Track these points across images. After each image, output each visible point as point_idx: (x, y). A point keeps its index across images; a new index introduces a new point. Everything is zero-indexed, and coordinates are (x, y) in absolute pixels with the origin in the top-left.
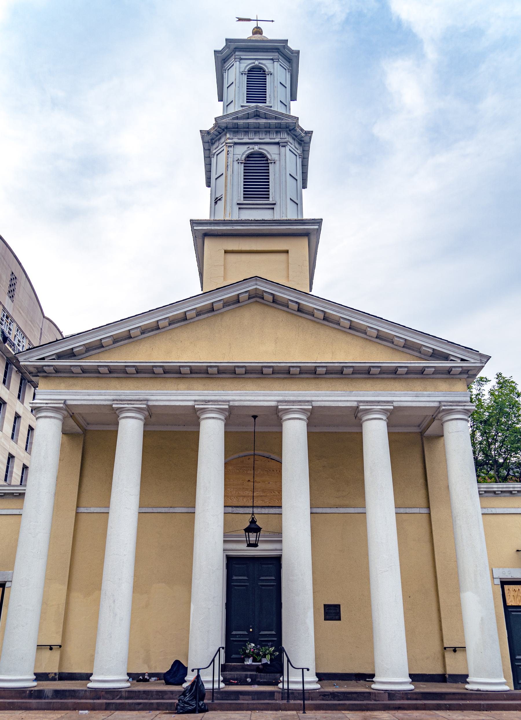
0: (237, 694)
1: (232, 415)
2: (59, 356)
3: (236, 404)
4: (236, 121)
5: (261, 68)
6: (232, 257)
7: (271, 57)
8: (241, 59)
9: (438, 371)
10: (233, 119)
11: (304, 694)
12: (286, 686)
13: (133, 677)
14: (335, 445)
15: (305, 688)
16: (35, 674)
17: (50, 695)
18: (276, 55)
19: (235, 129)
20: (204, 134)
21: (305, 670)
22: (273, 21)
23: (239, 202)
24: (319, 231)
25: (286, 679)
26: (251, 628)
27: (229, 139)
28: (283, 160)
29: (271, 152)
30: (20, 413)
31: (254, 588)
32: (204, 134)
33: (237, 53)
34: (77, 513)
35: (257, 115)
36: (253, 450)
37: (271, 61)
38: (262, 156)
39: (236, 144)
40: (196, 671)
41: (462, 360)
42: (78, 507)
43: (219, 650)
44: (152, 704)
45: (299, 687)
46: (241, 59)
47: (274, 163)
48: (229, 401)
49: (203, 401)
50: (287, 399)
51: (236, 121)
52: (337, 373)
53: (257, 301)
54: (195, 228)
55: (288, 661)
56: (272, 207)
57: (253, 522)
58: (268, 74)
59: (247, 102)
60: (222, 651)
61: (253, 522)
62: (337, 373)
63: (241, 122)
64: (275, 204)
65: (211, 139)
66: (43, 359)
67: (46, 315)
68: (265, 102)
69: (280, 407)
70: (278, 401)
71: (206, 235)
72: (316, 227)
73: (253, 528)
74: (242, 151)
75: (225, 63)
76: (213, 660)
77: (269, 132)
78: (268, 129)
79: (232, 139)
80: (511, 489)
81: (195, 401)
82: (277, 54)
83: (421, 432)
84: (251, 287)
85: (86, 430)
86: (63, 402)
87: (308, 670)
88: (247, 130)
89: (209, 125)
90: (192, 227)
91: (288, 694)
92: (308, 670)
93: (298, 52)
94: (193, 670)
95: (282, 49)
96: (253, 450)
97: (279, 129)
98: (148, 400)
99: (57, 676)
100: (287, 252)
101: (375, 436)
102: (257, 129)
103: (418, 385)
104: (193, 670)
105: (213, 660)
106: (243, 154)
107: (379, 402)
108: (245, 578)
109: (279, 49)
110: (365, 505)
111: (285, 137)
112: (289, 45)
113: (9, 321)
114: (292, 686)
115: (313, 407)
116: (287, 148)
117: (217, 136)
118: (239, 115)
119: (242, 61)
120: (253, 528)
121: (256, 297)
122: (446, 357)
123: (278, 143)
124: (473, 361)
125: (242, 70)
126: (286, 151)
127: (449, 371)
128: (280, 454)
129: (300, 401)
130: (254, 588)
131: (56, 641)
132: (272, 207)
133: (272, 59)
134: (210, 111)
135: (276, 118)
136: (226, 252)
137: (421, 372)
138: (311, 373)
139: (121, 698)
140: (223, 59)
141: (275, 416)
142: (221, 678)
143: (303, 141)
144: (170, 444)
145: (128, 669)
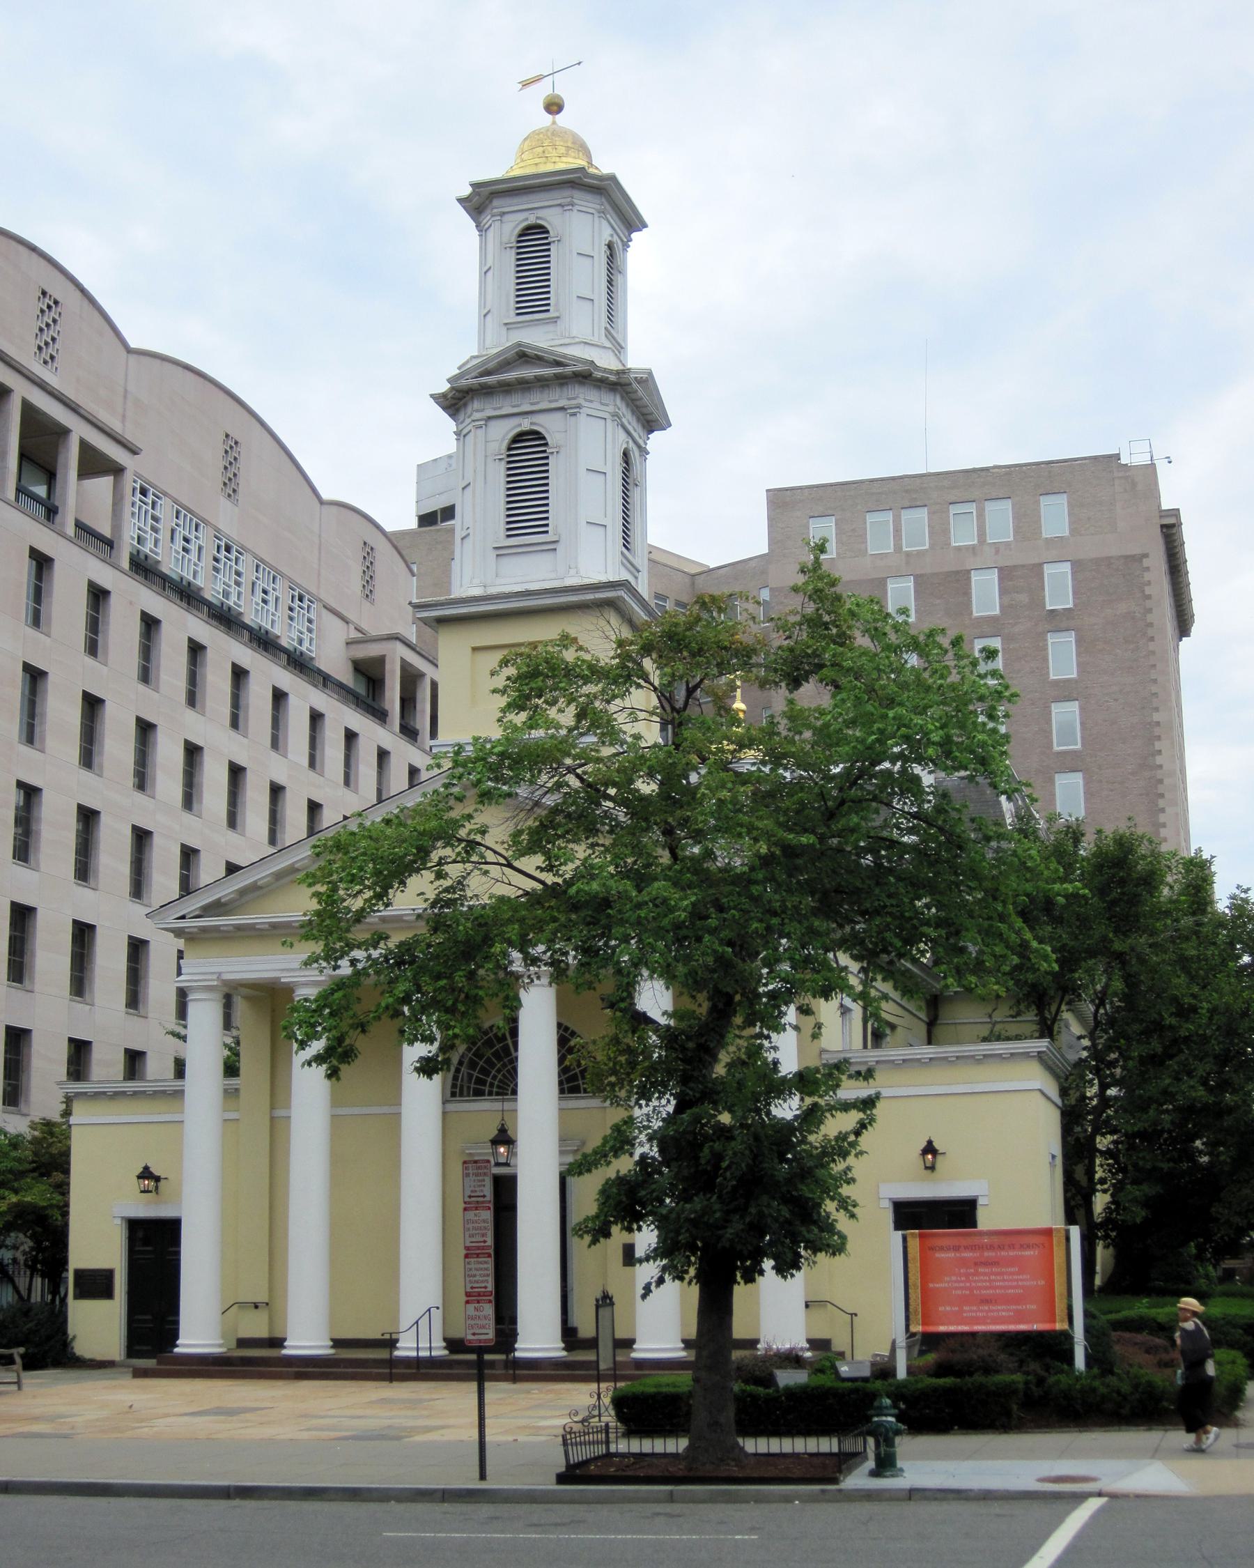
5: (541, 227)
7: (559, 202)
8: (503, 214)
10: (481, 375)
13: (338, 1343)
19: (486, 391)
27: (477, 411)
29: (549, 425)
30: (281, 780)
33: (496, 202)
34: (272, 1119)
35: (523, 356)
37: (558, 210)
38: (537, 435)
39: (490, 418)
42: (272, 1108)
46: (503, 214)
66: (183, 917)
67: (326, 496)
71: (441, 621)
74: (503, 431)
77: (548, 386)
78: (542, 383)
79: (483, 410)
82: (567, 192)
86: (215, 977)
88: (507, 388)
102: (524, 386)
106: (503, 440)
108: (149, 1317)
110: (561, 1117)
113: (233, 556)
119: (506, 218)
123: (562, 409)
125: (505, 239)
131: (262, 1297)
132: (551, 547)
136: (475, 649)
143: (638, 402)
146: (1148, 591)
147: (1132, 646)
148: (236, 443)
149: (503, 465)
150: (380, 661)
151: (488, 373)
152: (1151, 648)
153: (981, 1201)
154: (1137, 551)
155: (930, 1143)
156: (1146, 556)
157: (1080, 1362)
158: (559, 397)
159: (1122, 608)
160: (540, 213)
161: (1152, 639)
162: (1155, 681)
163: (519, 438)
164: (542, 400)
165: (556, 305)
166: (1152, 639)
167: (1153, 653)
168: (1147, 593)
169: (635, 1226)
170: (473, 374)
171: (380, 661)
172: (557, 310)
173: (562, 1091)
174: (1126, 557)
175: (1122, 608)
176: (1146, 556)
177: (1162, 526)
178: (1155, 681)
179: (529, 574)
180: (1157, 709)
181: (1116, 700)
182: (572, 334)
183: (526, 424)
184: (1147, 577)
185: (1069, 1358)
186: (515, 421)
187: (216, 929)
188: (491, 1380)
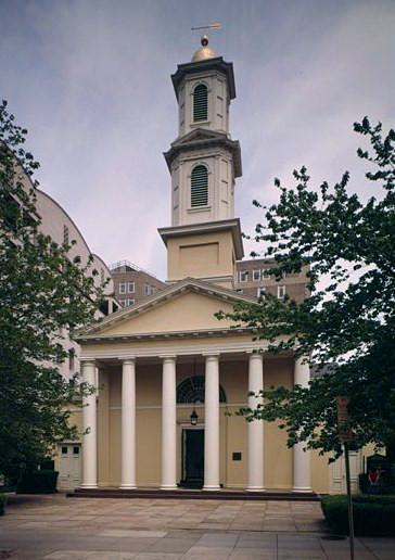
6: (183, 250)
18: (213, 72)
22: (255, 203)
24: (239, 225)
28: (219, 168)
29: (209, 163)
31: (193, 444)
36: (190, 389)
56: (209, 123)
57: (194, 413)
61: (194, 413)
65: (172, 157)
73: (194, 416)
78: (207, 146)
88: (192, 148)
89: (168, 148)
93: (237, 142)
96: (190, 389)
97: (213, 145)
100: (217, 243)
101: (129, 373)
102: (199, 147)
111: (219, 150)
112: (224, 59)
120: (194, 416)
123: (213, 157)
130: (193, 444)
134: (170, 135)
136: (181, 247)
140: (179, 80)
143: (233, 149)
144: (149, 373)
160: (205, 80)
182: (214, 124)
183: (199, 163)
187: (94, 340)
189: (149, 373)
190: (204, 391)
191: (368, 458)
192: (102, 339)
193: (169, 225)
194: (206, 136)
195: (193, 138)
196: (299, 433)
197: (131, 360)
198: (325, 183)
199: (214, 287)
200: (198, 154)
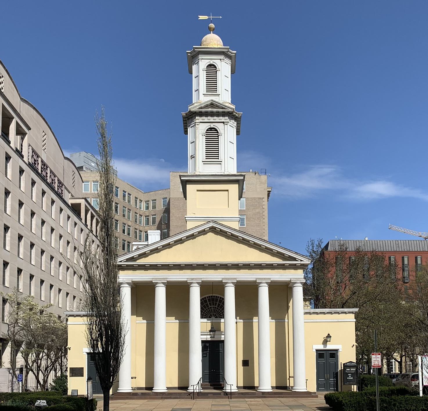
0: (207, 394)
1: (205, 286)
2: (128, 260)
3: (205, 280)
4: (200, 110)
5: (214, 65)
7: (220, 58)
9: (290, 265)
10: (199, 108)
11: (231, 393)
12: (225, 391)
13: (168, 388)
14: (247, 294)
15: (232, 391)
16: (166, 387)
17: (140, 394)
18: (222, 57)
20: (184, 118)
21: (232, 385)
23: (204, 93)
25: (225, 388)
26: (213, 370)
29: (220, 127)
31: (214, 351)
32: (184, 118)
35: (212, 105)
36: (212, 307)
39: (201, 122)
40: (193, 386)
41: (301, 260)
43: (200, 379)
44: (177, 397)
45: (230, 391)
47: (221, 135)
48: (202, 279)
49: (190, 278)
50: (226, 277)
51: (200, 110)
52: (247, 266)
53: (213, 230)
54: (182, 178)
55: (226, 382)
58: (218, 71)
59: (207, 92)
60: (201, 379)
62: (247, 266)
63: (203, 110)
64: (221, 162)
66: (121, 261)
68: (217, 92)
69: (223, 281)
70: (223, 279)
72: (242, 178)
74: (207, 126)
75: (193, 58)
76: (199, 382)
78: (218, 114)
80: (324, 311)
81: (187, 278)
83: (287, 285)
84: (211, 225)
85: (137, 285)
87: (233, 385)
88: (207, 114)
90: (180, 178)
91: (226, 394)
92: (233, 385)
94: (192, 386)
95: (226, 53)
96: (212, 307)
98: (167, 278)
99: (136, 388)
100: (228, 191)
102: (212, 114)
103: (281, 271)
104: (192, 386)
105: (199, 382)
107: (265, 279)
109: (224, 52)
110: (154, 319)
114: (227, 391)
115: (237, 281)
116: (228, 125)
117: (190, 116)
118: (203, 106)
121: (213, 230)
122: (295, 259)
123: (223, 122)
124: (305, 261)
126: (227, 127)
127: (295, 264)
128: (224, 295)
129: (231, 278)
130: (214, 351)
132: (220, 163)
133: (220, 59)
135: (222, 108)
137: (284, 265)
138: (236, 267)
139: (166, 395)
141: (220, 286)
142: (202, 388)
144: (178, 294)
145: (271, 385)
146: (264, 207)
147: (259, 220)
148: (45, 134)
149: (204, 137)
150: (79, 205)
151: (201, 108)
152: (264, 221)
153: (340, 350)
154: (262, 197)
155: (329, 334)
156: (264, 198)
157: (421, 394)
158: (222, 119)
159: (257, 210)
161: (264, 219)
162: (264, 229)
163: (211, 129)
164: (217, 119)
165: (219, 91)
166: (264, 219)
167: (264, 222)
168: (263, 207)
169: (7, 340)
170: (198, 108)
171: (79, 205)
172: (219, 92)
173: (201, 318)
174: (259, 198)
175: (257, 210)
176: (264, 198)
177: (268, 191)
178: (264, 229)
179: (212, 170)
180: (264, 236)
181: (255, 233)
183: (212, 125)
184: (264, 203)
185: (419, 394)
186: (209, 124)
188: (241, 387)
189: (178, 294)
190: (223, 309)
191: (344, 364)
192: (139, 265)
193: (235, 172)
194: (218, 107)
195: (207, 106)
196: (323, 257)
197: (128, 283)
198: (329, 336)
199: (222, 225)
200: (211, 119)
